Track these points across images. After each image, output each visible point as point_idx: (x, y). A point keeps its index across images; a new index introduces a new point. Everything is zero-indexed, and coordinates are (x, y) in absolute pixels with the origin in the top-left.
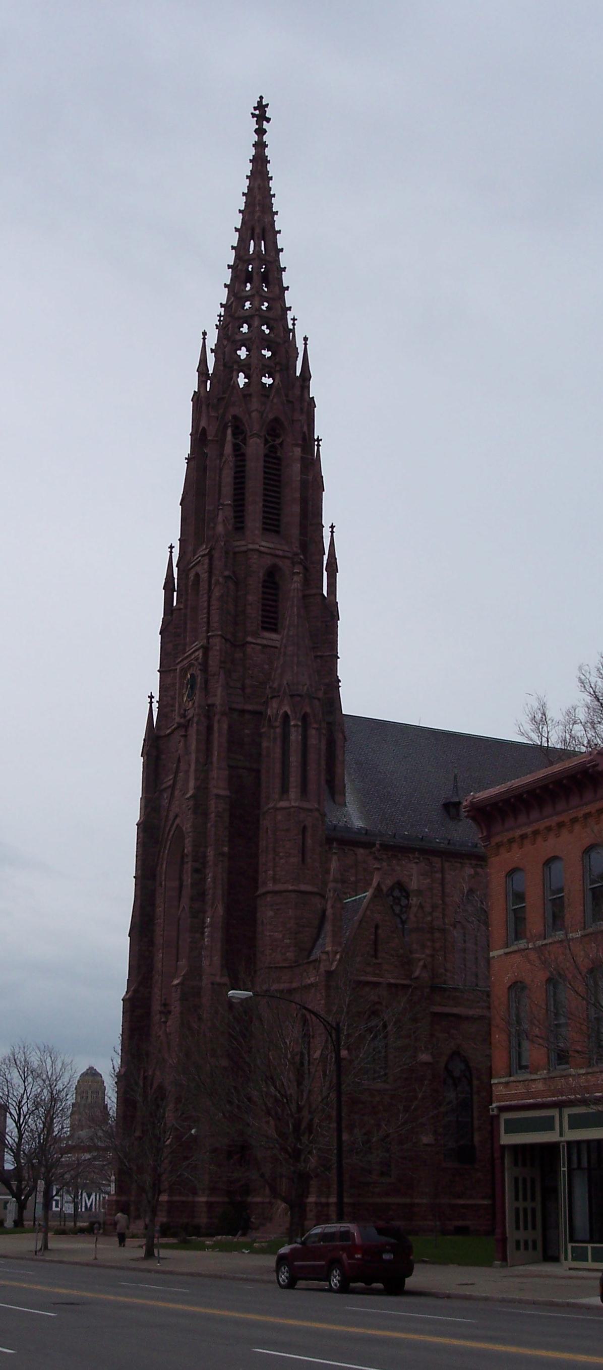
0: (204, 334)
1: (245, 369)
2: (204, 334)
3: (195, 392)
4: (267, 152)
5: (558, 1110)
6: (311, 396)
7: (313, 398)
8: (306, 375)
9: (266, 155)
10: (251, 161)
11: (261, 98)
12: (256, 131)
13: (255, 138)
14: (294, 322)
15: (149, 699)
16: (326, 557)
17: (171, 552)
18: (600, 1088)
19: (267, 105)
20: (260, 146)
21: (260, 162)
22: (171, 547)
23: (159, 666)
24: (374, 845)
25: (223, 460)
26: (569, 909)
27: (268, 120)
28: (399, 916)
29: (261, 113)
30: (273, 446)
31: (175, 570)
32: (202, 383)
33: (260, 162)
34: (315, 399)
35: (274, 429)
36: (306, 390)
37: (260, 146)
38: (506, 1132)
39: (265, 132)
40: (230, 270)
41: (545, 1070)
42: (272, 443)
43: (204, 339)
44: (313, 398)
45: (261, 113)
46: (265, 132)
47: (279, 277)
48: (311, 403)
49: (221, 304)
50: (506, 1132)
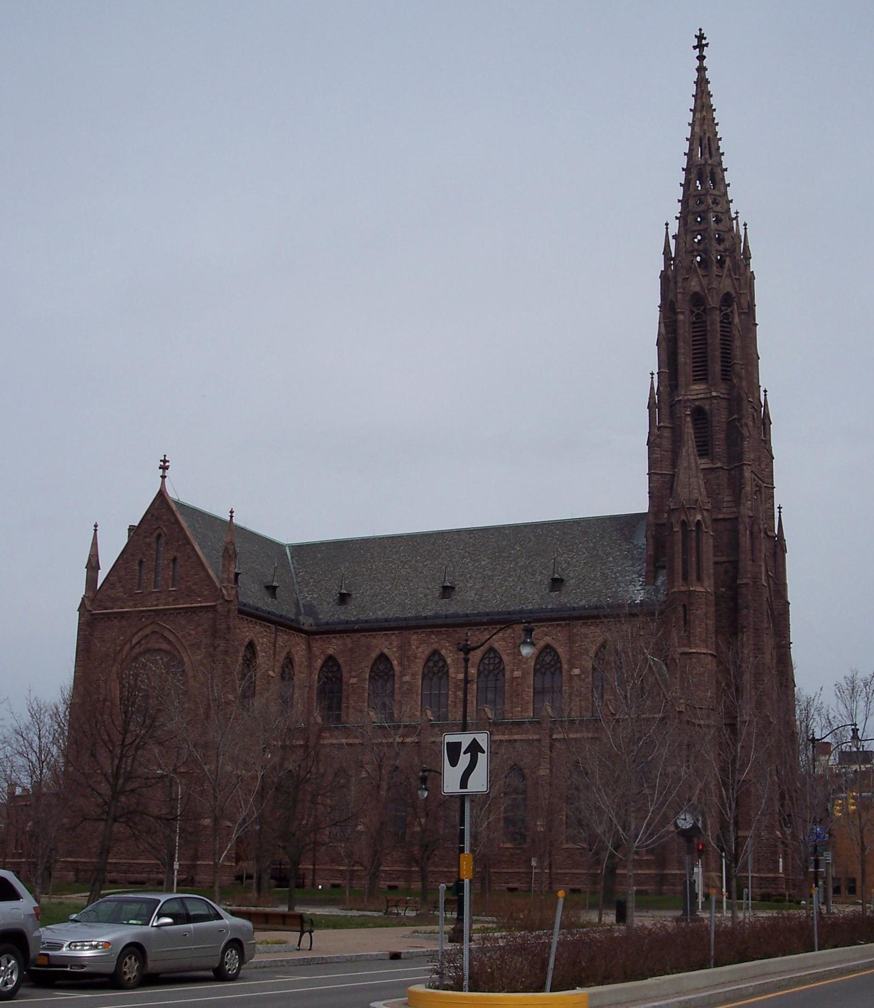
0: (667, 224)
1: (701, 253)
2: (667, 224)
3: (662, 271)
4: (708, 75)
6: (751, 271)
7: (753, 272)
8: (747, 257)
9: (707, 77)
14: (164, 472)
15: (651, 376)
16: (742, 244)
20: (701, 69)
21: (702, 83)
22: (652, 374)
23: (648, 470)
25: (616, 837)
30: (726, 314)
31: (673, 243)
32: (667, 266)
33: (702, 83)
34: (754, 273)
35: (727, 300)
36: (748, 267)
37: (701, 69)
38: (467, 788)
40: (684, 172)
41: (683, 922)
42: (725, 312)
43: (667, 228)
44: (753, 272)
45: (701, 43)
48: (752, 276)
49: (683, 168)
50: (467, 788)
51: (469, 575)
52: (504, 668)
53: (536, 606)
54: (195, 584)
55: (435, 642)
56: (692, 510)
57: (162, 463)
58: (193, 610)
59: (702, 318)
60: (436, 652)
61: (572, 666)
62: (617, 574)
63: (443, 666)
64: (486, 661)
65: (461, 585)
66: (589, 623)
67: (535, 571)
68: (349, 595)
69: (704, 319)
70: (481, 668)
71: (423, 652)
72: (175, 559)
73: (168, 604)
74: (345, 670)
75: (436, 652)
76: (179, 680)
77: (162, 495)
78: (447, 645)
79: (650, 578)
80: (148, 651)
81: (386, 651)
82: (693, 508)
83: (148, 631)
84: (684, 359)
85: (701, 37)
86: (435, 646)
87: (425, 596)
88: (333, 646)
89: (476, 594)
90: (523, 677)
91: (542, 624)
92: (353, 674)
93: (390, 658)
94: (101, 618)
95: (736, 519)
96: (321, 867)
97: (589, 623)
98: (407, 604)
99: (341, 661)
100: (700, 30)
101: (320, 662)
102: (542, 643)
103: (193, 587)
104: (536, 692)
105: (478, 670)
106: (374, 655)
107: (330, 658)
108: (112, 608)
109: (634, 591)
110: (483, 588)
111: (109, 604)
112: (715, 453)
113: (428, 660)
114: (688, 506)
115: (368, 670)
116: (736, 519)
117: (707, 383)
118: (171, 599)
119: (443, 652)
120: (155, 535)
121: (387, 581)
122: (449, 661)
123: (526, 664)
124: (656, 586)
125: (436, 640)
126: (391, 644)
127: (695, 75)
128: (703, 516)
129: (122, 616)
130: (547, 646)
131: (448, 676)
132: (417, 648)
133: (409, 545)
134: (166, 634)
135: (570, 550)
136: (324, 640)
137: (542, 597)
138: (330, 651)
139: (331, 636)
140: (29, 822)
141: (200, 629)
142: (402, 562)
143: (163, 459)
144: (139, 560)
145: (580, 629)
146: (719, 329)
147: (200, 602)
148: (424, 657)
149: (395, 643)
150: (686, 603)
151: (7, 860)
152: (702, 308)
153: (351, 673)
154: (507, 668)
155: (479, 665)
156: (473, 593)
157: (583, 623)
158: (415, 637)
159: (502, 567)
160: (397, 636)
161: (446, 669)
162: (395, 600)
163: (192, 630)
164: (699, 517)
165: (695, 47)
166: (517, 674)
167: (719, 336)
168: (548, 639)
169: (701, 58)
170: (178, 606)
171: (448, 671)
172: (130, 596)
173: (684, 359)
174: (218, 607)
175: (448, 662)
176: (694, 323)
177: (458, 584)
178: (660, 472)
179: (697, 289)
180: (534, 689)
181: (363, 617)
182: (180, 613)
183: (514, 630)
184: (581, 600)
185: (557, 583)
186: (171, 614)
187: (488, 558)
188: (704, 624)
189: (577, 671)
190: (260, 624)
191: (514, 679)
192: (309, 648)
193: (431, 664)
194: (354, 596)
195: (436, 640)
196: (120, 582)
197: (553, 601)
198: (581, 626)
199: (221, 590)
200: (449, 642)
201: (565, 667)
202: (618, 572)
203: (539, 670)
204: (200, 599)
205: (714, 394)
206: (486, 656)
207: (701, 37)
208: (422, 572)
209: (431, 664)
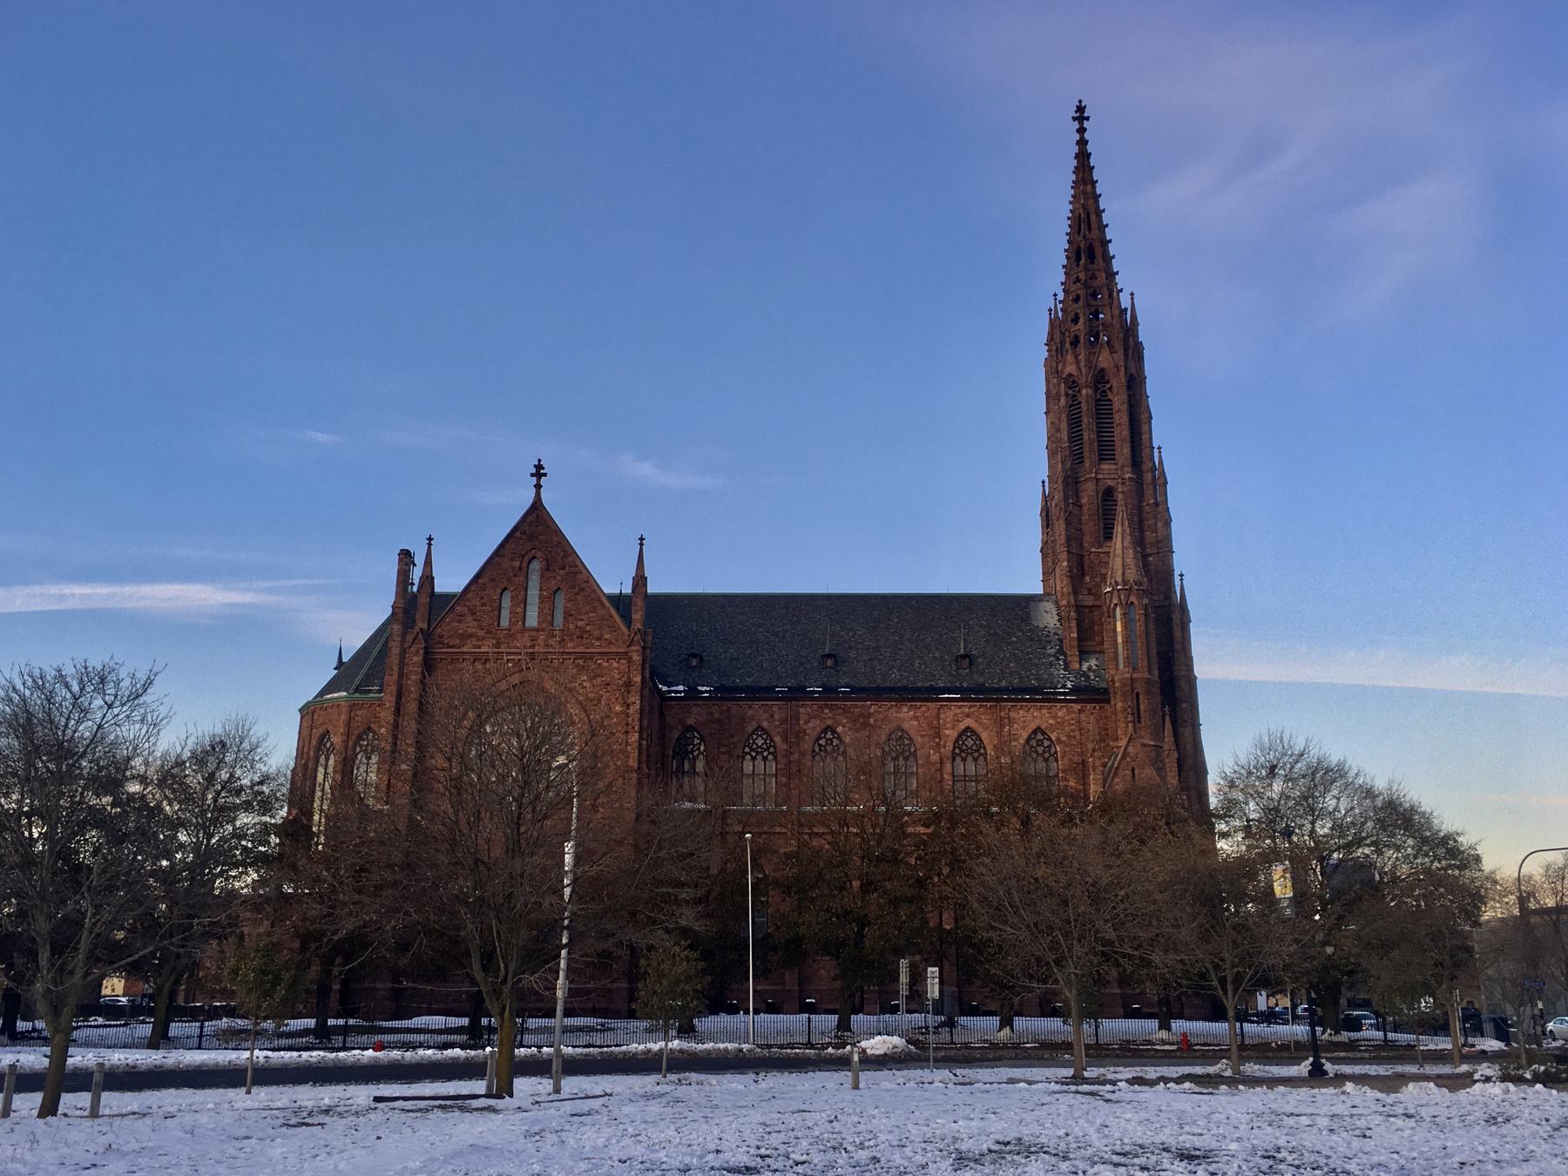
4: (1089, 148)
5: (652, 589)
10: (1074, 172)
11: (1080, 101)
12: (1078, 131)
13: (1076, 150)
14: (539, 480)
17: (1044, 486)
18: (583, 617)
19: (1085, 106)
20: (1082, 143)
21: (1083, 156)
22: (1043, 482)
24: (934, 1049)
26: (347, 898)
27: (1087, 118)
28: (1042, 755)
29: (1081, 115)
33: (1083, 156)
37: (1082, 143)
39: (1085, 130)
45: (1081, 115)
46: (1085, 130)
47: (1187, 1011)
71: (813, 728)
77: (537, 507)
78: (845, 721)
81: (765, 724)
85: (539, 467)
86: (829, 722)
92: (723, 749)
100: (539, 461)
102: (962, 726)
103: (588, 628)
119: (840, 729)
122: (847, 740)
125: (830, 715)
126: (772, 716)
130: (968, 729)
132: (806, 723)
139: (691, 703)
149: (776, 716)
151: (331, 1022)
165: (532, 475)
168: (968, 722)
169: (1082, 130)
184: (1000, 681)
193: (1034, 743)
195: (830, 715)
200: (846, 718)
203: (959, 755)
207: (539, 467)
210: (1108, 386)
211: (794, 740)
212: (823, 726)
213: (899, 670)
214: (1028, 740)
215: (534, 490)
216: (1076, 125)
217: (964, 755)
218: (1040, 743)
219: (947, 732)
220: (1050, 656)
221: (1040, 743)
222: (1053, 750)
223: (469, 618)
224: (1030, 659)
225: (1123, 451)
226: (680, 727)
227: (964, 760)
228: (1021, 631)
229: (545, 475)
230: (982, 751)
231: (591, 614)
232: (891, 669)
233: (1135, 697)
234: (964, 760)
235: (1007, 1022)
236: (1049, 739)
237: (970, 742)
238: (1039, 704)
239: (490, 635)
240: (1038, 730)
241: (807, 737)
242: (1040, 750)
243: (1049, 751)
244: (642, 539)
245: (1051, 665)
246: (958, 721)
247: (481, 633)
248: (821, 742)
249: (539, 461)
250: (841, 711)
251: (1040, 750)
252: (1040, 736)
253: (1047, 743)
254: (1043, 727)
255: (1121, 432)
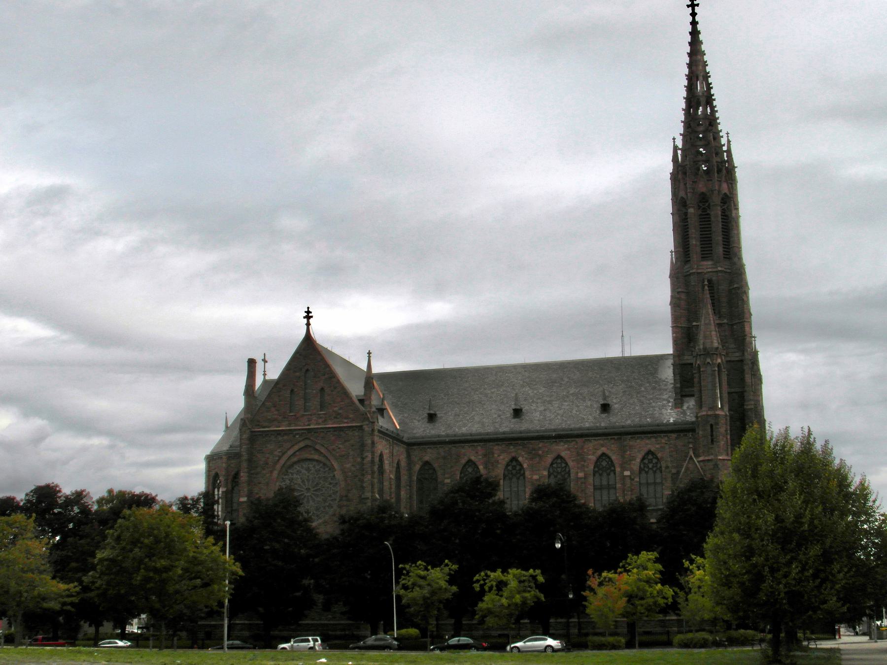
4: (699, 27)
20: (694, 23)
21: (695, 33)
28: (652, 469)
33: (695, 33)
37: (694, 23)
51: (531, 400)
52: (569, 471)
53: (592, 424)
54: (341, 408)
55: (513, 451)
56: (715, 356)
57: (306, 314)
58: (341, 429)
59: (706, 211)
60: (514, 459)
61: (624, 469)
62: (651, 401)
63: (520, 470)
64: (555, 465)
65: (527, 408)
66: (636, 438)
67: (585, 398)
68: (435, 415)
69: (708, 212)
70: (551, 471)
71: (504, 459)
72: (322, 389)
73: (319, 424)
74: (439, 473)
75: (514, 459)
76: (330, 484)
79: (678, 403)
80: (299, 461)
81: (473, 458)
82: (715, 354)
83: (302, 445)
84: (694, 242)
86: (513, 454)
87: (499, 416)
88: (429, 455)
89: (540, 415)
90: (585, 478)
91: (598, 438)
93: (477, 463)
94: (260, 435)
95: (742, 361)
96: (443, 622)
97: (636, 438)
98: (486, 423)
99: (435, 465)
100: (308, 308)
101: (417, 467)
102: (599, 453)
103: (340, 411)
104: (595, 488)
105: (549, 472)
106: (463, 461)
107: (427, 463)
108: (268, 427)
109: (666, 413)
110: (545, 410)
111: (266, 424)
112: (722, 313)
113: (508, 465)
114: (712, 353)
115: (458, 473)
116: (742, 361)
117: (712, 260)
118: (320, 421)
119: (520, 459)
120: (304, 370)
121: (464, 404)
122: (525, 466)
123: (587, 468)
124: (683, 410)
126: (477, 453)
127: (690, 28)
128: (722, 360)
129: (279, 433)
130: (603, 454)
131: (524, 478)
133: (475, 376)
134: (317, 447)
135: (609, 382)
136: (421, 450)
137: (595, 418)
138: (427, 458)
140: (865, 612)
141: (347, 444)
142: (473, 389)
143: (307, 310)
144: (291, 389)
145: (629, 442)
146: (720, 220)
147: (347, 423)
148: (505, 463)
149: (480, 453)
150: (713, 423)
152: (707, 204)
153: (444, 475)
154: (572, 471)
155: (549, 469)
156: (538, 414)
157: (631, 437)
158: (496, 447)
159: (557, 394)
160: (481, 447)
161: (522, 472)
162: (474, 419)
163: (341, 444)
164: (719, 361)
166: (581, 475)
167: (721, 226)
168: (603, 450)
169: (694, 14)
170: (327, 426)
171: (524, 473)
172: (284, 418)
173: (694, 242)
174: (364, 427)
175: (525, 467)
176: (701, 215)
177: (525, 407)
178: (680, 325)
179: (704, 190)
180: (594, 486)
181: (450, 432)
182: (329, 431)
183: (577, 442)
184: (626, 420)
185: (605, 408)
186: (321, 432)
187: (544, 387)
188: (725, 438)
189: (627, 473)
190: (383, 438)
191: (578, 479)
192: (409, 456)
193: (510, 468)
194: (439, 416)
196: (275, 407)
197: (605, 422)
198: (629, 439)
199: (366, 414)
201: (618, 469)
202: (652, 399)
203: (597, 472)
204: (346, 421)
205: (720, 269)
206: (554, 462)
208: (491, 397)
209: (510, 468)
210: (707, 204)
211: (491, 467)
212: (510, 457)
213: (562, 416)
214: (643, 459)
215: (263, 376)
216: (690, 10)
217: (601, 472)
218: (650, 461)
219: (589, 457)
220: (664, 400)
221: (650, 461)
222: (659, 466)
223: (273, 409)
224: (650, 404)
225: (719, 250)
226: (420, 462)
227: (647, 473)
228: (649, 382)
229: (312, 317)
230: (613, 468)
231: (341, 403)
232: (556, 416)
233: (709, 428)
234: (601, 475)
235: (217, 502)
236: (657, 458)
237: (604, 464)
238: (649, 435)
239: (286, 419)
240: (649, 452)
241: (499, 466)
242: (650, 466)
243: (656, 466)
244: (369, 353)
245: (664, 406)
246: (596, 449)
247: (280, 418)
248: (554, 466)
249: (308, 308)
250: (521, 447)
251: (650, 466)
252: (650, 457)
253: (655, 461)
254: (652, 450)
255: (718, 238)
